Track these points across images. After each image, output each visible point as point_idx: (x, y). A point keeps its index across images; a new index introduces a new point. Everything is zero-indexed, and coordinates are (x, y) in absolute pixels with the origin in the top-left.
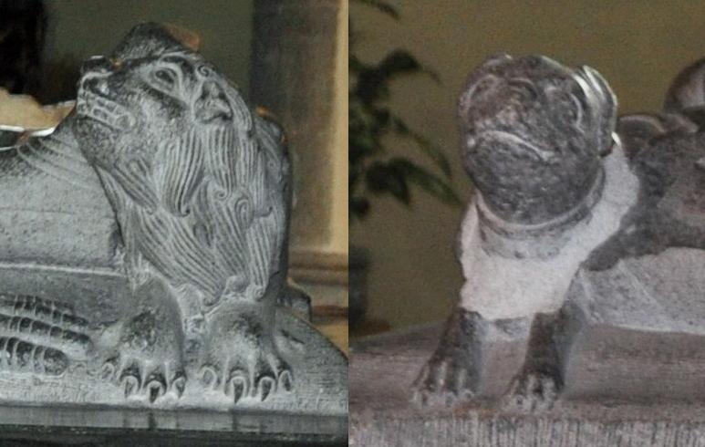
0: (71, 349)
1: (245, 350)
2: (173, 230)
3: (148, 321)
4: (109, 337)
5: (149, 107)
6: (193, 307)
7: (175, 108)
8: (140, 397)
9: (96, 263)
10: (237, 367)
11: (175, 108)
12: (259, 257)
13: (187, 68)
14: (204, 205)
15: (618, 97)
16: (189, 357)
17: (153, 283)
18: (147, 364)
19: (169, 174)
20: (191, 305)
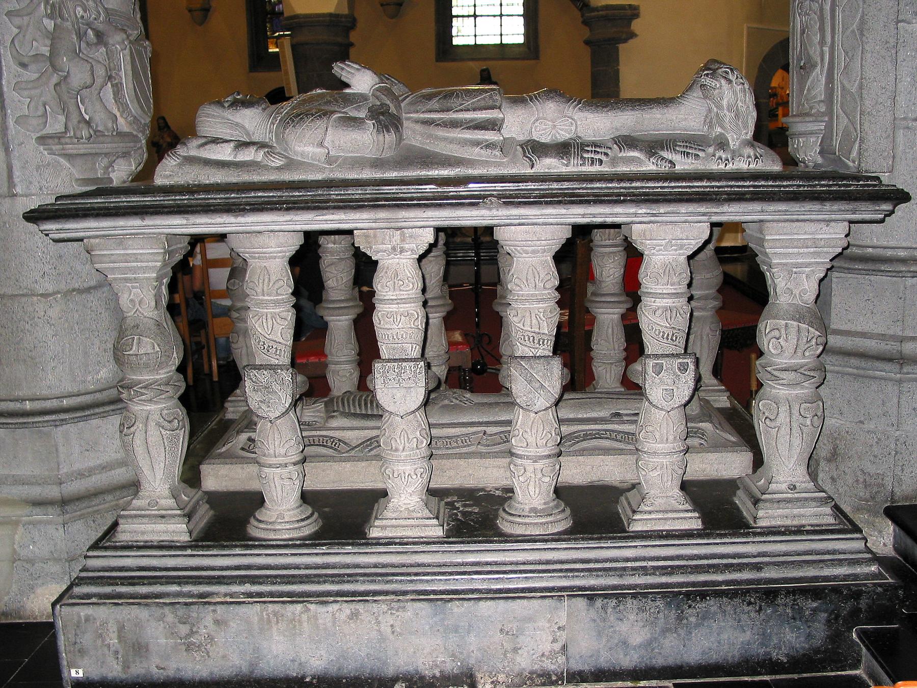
0: (701, 154)
1: (749, 151)
2: (728, 116)
3: (722, 144)
4: (711, 150)
5: (723, 82)
6: (733, 140)
7: (730, 81)
8: (722, 166)
9: (699, 130)
10: (749, 157)
11: (730, 81)
12: (248, 588)
13: (732, 70)
14: (737, 109)
15: (424, 88)
16: (735, 154)
17: (721, 134)
18: (724, 156)
19: (728, 102)
20: (734, 141)
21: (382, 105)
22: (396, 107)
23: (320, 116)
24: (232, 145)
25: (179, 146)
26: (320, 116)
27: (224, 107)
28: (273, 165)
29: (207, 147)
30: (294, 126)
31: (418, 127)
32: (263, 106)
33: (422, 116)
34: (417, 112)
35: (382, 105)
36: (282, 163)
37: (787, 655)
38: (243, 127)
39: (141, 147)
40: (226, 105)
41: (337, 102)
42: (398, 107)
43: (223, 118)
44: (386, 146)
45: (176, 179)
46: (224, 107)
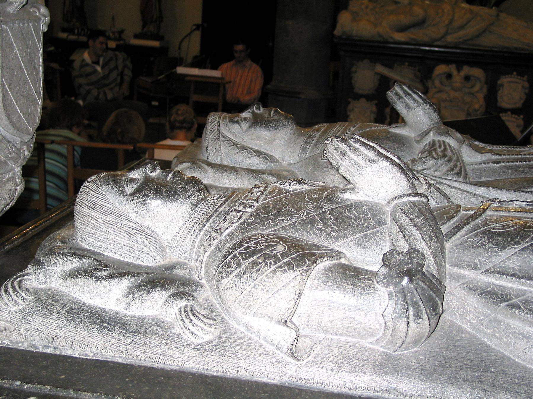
21: (412, 252)
22: (435, 257)
23: (289, 264)
24: (125, 283)
25: (30, 269)
26: (289, 264)
27: (123, 192)
28: (192, 339)
29: (80, 281)
30: (238, 276)
31: (474, 302)
32: (194, 199)
33: (484, 278)
34: (475, 267)
35: (412, 252)
36: (208, 338)
37: (502, 85)
38: (151, 236)
39: (12, 178)
40: (129, 189)
41: (325, 221)
42: (440, 255)
43: (119, 215)
44: (408, 340)
45: (14, 337)
46: (123, 192)
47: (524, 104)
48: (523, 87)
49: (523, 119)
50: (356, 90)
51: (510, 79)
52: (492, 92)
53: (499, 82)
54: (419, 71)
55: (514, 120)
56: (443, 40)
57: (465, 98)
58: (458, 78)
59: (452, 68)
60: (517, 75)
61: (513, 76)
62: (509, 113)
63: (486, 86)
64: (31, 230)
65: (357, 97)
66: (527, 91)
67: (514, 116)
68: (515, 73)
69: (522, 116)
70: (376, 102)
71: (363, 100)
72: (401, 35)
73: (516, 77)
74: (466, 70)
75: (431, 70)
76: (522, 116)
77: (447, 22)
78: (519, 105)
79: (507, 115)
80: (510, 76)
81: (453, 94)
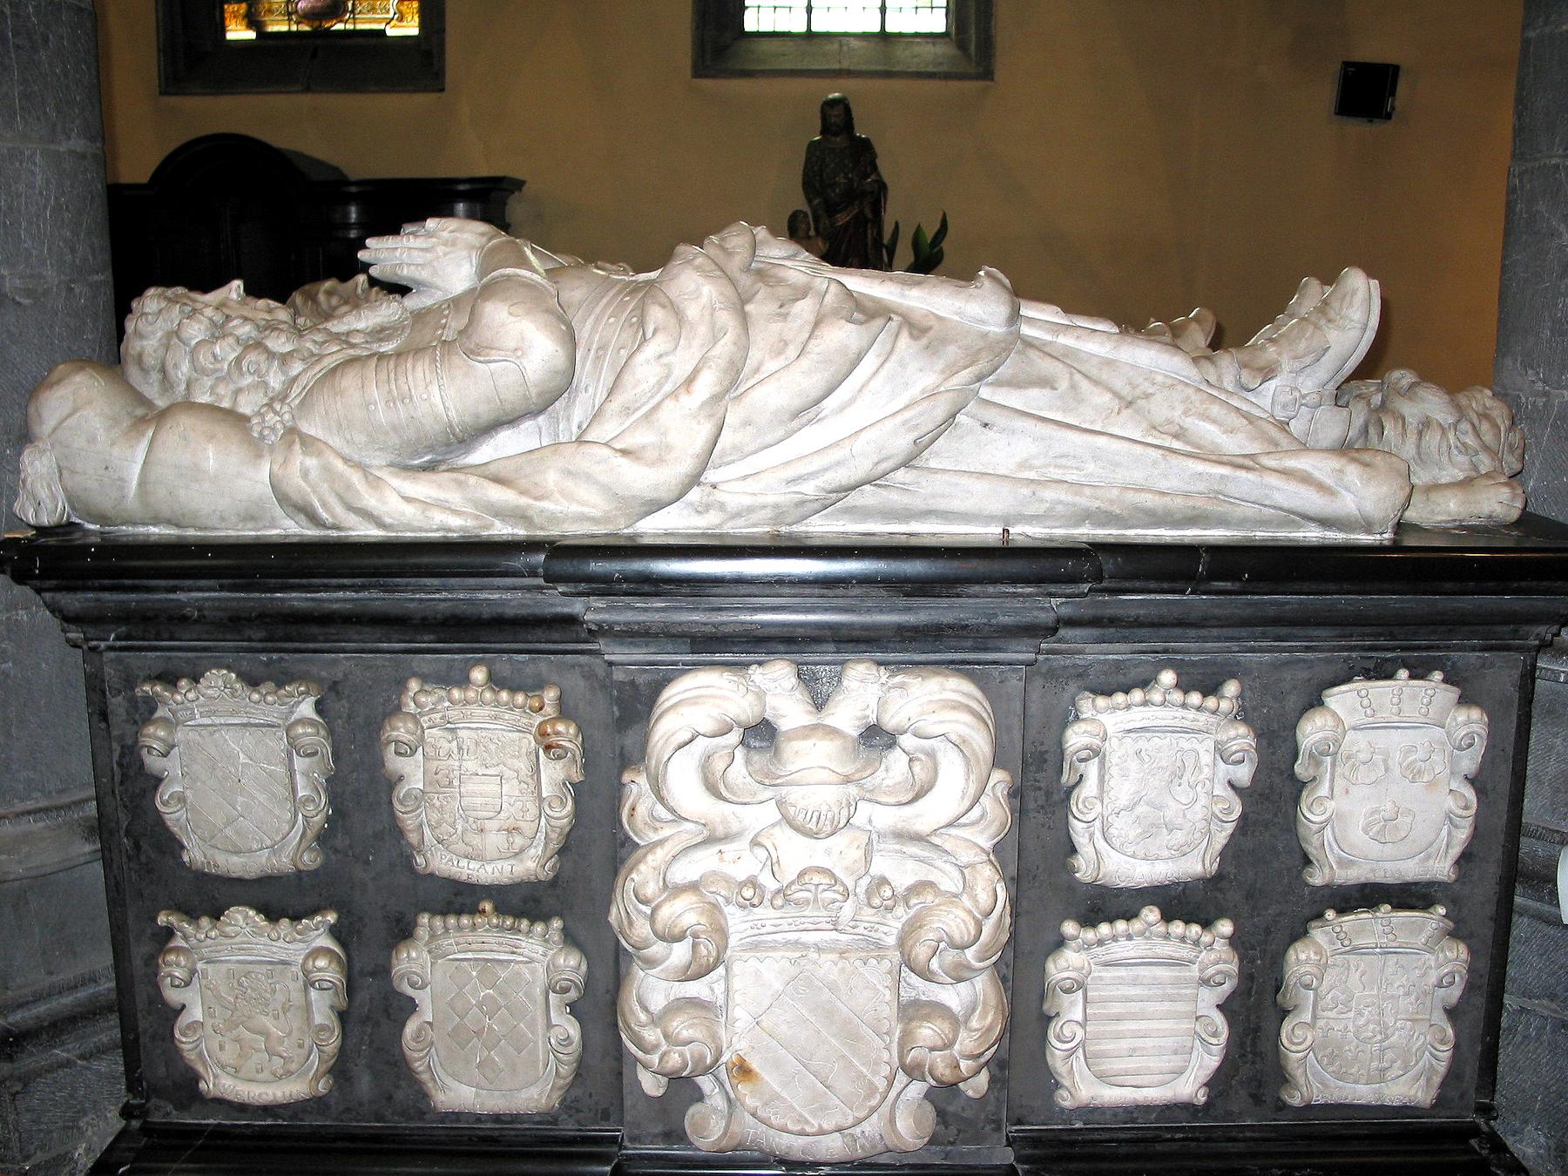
47: (1230, 853)
48: (1221, 752)
49: (1233, 941)
50: (196, 853)
51: (1138, 717)
52: (1038, 790)
53: (1075, 738)
54: (565, 711)
55: (1185, 952)
56: (694, 495)
57: (882, 865)
58: (813, 763)
59: (774, 685)
60: (1184, 686)
61: (1157, 697)
62: (1151, 914)
63: (999, 776)
64: (250, 640)
65: (211, 896)
66: (1244, 774)
67: (1178, 927)
68: (1168, 677)
69: (1225, 927)
70: (331, 918)
71: (242, 918)
72: (422, 488)
73: (1177, 696)
74: (864, 689)
75: (634, 707)
76: (1225, 927)
77: (330, 442)
78: (1196, 864)
79: (1136, 925)
80: (1137, 695)
81: (796, 853)
